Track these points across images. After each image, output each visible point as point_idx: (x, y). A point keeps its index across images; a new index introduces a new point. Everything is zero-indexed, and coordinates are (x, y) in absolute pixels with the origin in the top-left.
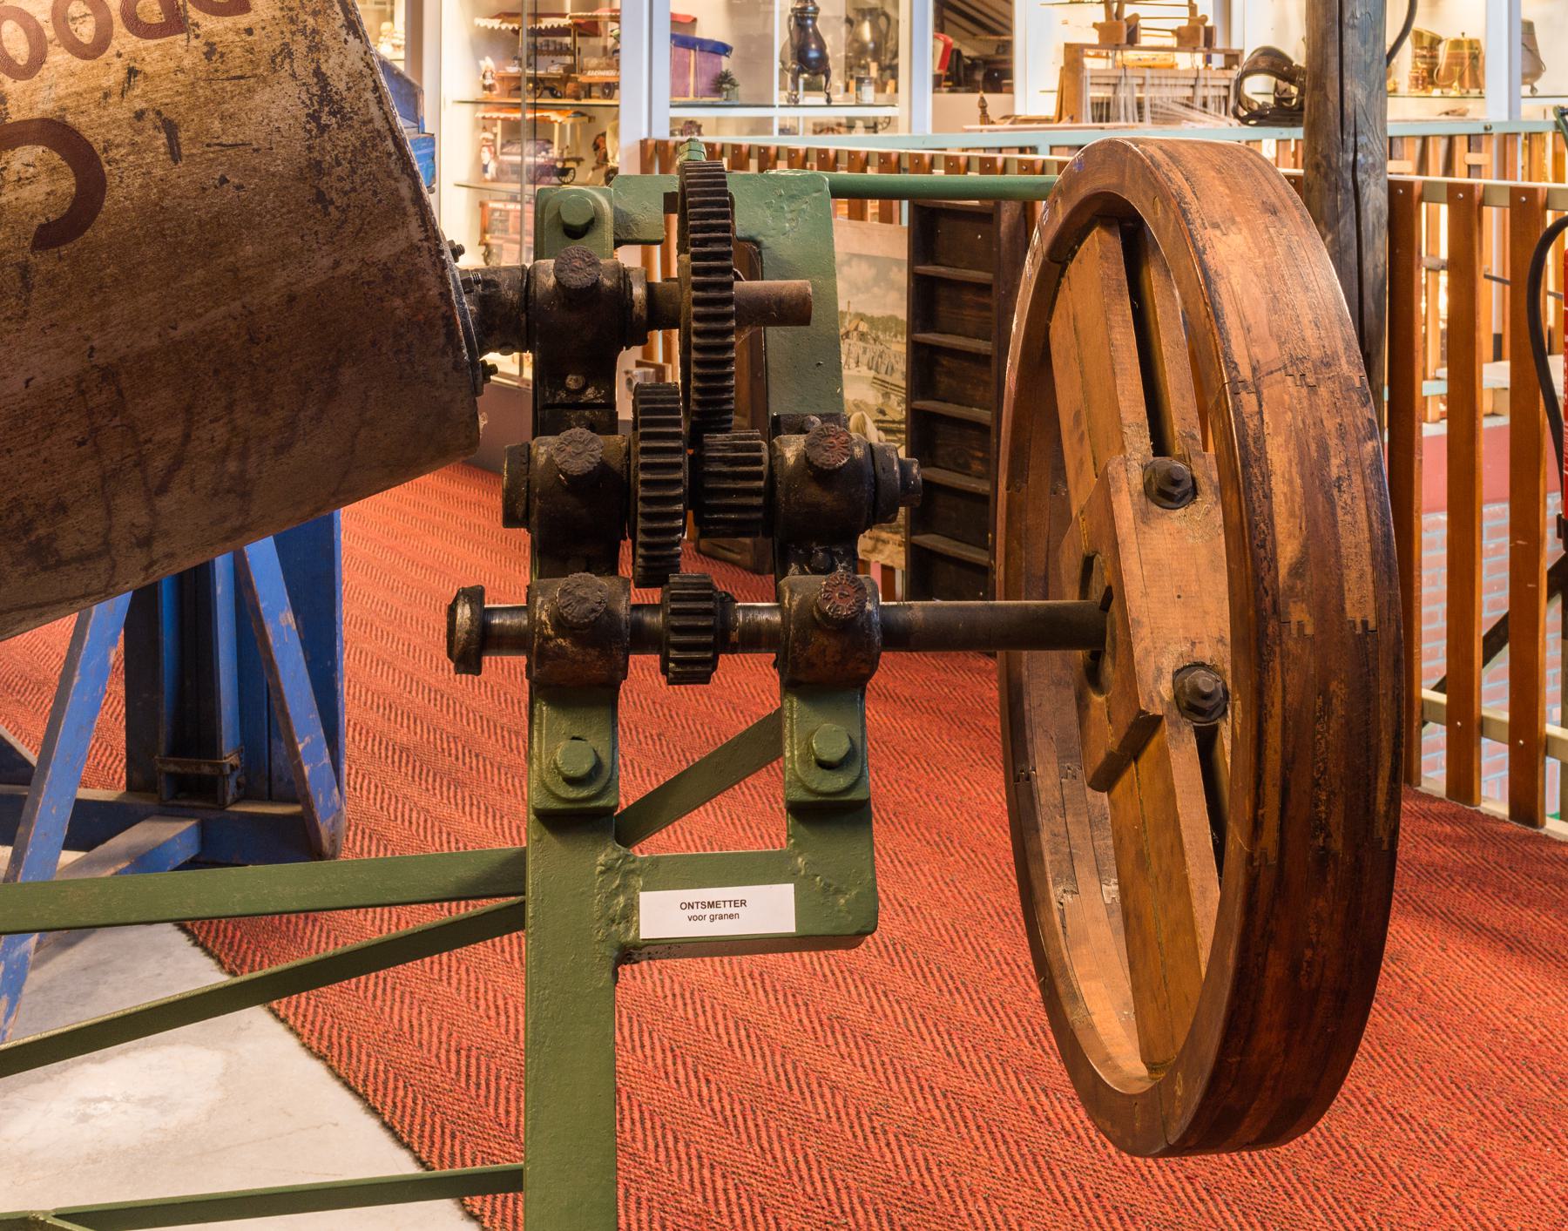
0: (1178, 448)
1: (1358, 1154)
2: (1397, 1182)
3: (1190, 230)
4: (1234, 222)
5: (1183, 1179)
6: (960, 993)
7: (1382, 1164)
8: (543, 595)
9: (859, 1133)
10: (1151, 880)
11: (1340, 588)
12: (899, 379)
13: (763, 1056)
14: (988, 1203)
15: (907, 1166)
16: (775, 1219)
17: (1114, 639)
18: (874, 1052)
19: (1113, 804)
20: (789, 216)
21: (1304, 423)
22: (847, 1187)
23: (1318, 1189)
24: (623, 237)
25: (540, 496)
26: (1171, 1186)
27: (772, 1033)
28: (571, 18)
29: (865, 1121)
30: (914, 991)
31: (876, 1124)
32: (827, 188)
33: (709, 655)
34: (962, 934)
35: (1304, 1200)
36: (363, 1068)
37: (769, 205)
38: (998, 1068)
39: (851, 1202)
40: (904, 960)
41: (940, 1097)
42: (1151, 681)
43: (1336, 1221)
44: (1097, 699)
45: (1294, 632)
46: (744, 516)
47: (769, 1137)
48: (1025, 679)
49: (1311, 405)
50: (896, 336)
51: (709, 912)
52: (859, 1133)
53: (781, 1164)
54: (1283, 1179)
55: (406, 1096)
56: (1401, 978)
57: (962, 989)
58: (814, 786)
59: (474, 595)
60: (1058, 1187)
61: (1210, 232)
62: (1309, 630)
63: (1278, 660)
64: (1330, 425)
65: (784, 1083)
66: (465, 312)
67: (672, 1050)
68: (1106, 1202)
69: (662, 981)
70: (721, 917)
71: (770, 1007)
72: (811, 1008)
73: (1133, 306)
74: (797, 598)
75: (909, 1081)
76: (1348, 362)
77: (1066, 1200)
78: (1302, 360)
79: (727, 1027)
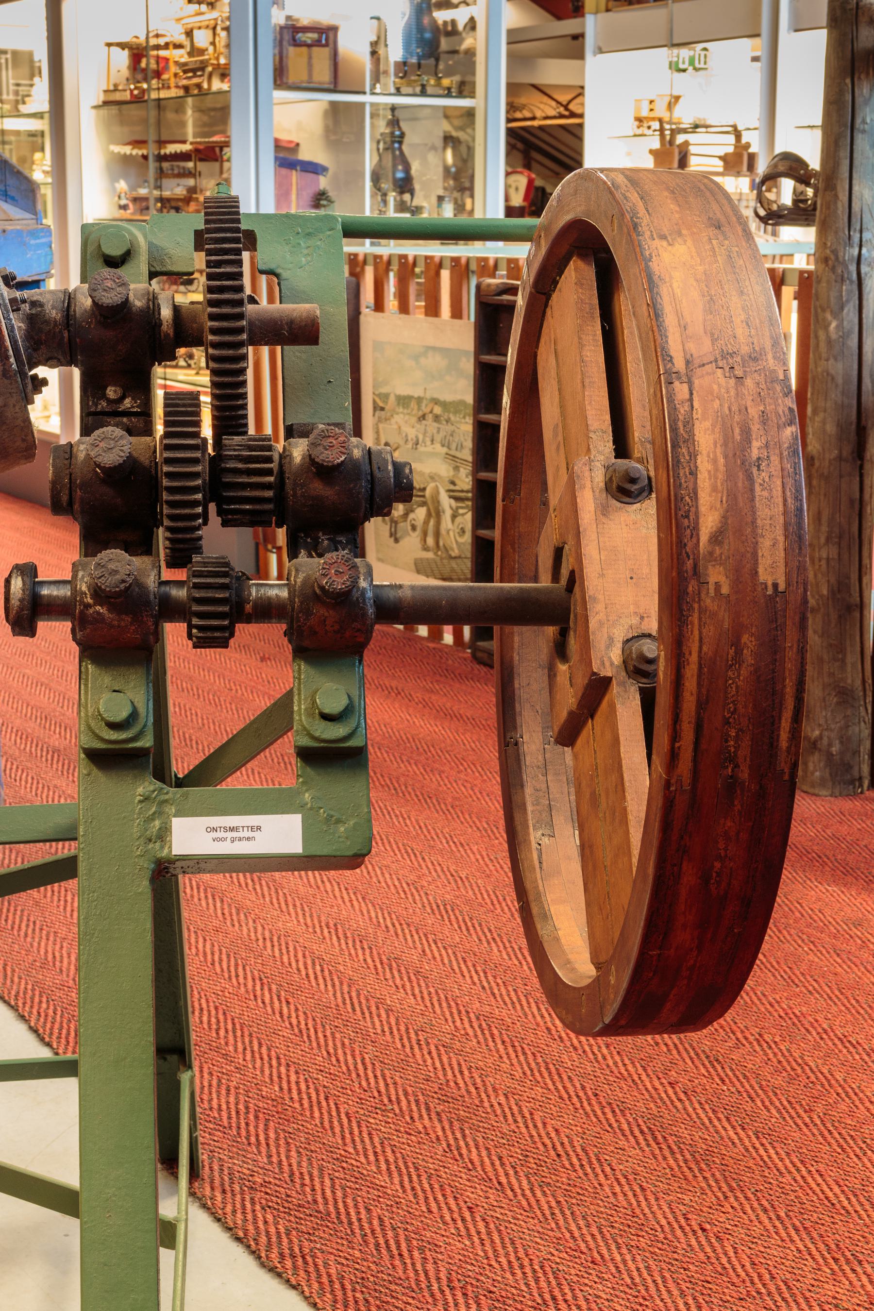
0: (637, 450)
1: (811, 1069)
2: (840, 1091)
3: (639, 241)
4: (680, 234)
5: (666, 1084)
6: (496, 942)
7: (830, 1077)
8: (84, 570)
9: (407, 1044)
10: (601, 815)
11: (755, 555)
12: (467, 454)
13: (334, 986)
14: (507, 1097)
15: (444, 1069)
16: (336, 1104)
17: (576, 616)
18: (423, 985)
19: (575, 757)
20: (305, 252)
21: (730, 410)
22: (395, 1083)
23: (776, 1094)
24: (158, 269)
25: (82, 486)
26: (656, 1089)
27: (341, 968)
28: (191, 143)
29: (413, 1035)
30: (458, 939)
31: (421, 1038)
32: (339, 227)
33: (226, 622)
34: (501, 898)
35: (763, 1102)
36: (15, 987)
37: (287, 242)
38: (523, 999)
39: (397, 1094)
40: (452, 917)
41: (473, 1019)
42: (602, 646)
43: (788, 1118)
44: (562, 668)
45: (712, 592)
46: (258, 507)
47: (335, 1045)
48: (516, 662)
49: (737, 394)
50: (464, 417)
51: (230, 835)
52: (407, 1044)
53: (343, 1065)
54: (748, 1087)
55: (48, 1008)
56: (860, 938)
57: (498, 939)
58: (317, 734)
59: (28, 571)
60: (564, 1087)
61: (657, 243)
62: (725, 590)
63: (696, 615)
64: (754, 412)
65: (349, 1006)
66: (13, 327)
67: (261, 979)
68: (602, 1099)
69: (255, 928)
70: (240, 839)
71: (342, 950)
72: (374, 951)
73: (603, 327)
74: (301, 576)
75: (450, 1007)
76: (774, 358)
77: (570, 1097)
78: (732, 355)
79: (305, 964)
